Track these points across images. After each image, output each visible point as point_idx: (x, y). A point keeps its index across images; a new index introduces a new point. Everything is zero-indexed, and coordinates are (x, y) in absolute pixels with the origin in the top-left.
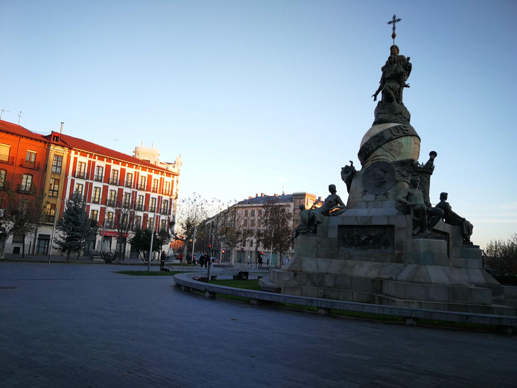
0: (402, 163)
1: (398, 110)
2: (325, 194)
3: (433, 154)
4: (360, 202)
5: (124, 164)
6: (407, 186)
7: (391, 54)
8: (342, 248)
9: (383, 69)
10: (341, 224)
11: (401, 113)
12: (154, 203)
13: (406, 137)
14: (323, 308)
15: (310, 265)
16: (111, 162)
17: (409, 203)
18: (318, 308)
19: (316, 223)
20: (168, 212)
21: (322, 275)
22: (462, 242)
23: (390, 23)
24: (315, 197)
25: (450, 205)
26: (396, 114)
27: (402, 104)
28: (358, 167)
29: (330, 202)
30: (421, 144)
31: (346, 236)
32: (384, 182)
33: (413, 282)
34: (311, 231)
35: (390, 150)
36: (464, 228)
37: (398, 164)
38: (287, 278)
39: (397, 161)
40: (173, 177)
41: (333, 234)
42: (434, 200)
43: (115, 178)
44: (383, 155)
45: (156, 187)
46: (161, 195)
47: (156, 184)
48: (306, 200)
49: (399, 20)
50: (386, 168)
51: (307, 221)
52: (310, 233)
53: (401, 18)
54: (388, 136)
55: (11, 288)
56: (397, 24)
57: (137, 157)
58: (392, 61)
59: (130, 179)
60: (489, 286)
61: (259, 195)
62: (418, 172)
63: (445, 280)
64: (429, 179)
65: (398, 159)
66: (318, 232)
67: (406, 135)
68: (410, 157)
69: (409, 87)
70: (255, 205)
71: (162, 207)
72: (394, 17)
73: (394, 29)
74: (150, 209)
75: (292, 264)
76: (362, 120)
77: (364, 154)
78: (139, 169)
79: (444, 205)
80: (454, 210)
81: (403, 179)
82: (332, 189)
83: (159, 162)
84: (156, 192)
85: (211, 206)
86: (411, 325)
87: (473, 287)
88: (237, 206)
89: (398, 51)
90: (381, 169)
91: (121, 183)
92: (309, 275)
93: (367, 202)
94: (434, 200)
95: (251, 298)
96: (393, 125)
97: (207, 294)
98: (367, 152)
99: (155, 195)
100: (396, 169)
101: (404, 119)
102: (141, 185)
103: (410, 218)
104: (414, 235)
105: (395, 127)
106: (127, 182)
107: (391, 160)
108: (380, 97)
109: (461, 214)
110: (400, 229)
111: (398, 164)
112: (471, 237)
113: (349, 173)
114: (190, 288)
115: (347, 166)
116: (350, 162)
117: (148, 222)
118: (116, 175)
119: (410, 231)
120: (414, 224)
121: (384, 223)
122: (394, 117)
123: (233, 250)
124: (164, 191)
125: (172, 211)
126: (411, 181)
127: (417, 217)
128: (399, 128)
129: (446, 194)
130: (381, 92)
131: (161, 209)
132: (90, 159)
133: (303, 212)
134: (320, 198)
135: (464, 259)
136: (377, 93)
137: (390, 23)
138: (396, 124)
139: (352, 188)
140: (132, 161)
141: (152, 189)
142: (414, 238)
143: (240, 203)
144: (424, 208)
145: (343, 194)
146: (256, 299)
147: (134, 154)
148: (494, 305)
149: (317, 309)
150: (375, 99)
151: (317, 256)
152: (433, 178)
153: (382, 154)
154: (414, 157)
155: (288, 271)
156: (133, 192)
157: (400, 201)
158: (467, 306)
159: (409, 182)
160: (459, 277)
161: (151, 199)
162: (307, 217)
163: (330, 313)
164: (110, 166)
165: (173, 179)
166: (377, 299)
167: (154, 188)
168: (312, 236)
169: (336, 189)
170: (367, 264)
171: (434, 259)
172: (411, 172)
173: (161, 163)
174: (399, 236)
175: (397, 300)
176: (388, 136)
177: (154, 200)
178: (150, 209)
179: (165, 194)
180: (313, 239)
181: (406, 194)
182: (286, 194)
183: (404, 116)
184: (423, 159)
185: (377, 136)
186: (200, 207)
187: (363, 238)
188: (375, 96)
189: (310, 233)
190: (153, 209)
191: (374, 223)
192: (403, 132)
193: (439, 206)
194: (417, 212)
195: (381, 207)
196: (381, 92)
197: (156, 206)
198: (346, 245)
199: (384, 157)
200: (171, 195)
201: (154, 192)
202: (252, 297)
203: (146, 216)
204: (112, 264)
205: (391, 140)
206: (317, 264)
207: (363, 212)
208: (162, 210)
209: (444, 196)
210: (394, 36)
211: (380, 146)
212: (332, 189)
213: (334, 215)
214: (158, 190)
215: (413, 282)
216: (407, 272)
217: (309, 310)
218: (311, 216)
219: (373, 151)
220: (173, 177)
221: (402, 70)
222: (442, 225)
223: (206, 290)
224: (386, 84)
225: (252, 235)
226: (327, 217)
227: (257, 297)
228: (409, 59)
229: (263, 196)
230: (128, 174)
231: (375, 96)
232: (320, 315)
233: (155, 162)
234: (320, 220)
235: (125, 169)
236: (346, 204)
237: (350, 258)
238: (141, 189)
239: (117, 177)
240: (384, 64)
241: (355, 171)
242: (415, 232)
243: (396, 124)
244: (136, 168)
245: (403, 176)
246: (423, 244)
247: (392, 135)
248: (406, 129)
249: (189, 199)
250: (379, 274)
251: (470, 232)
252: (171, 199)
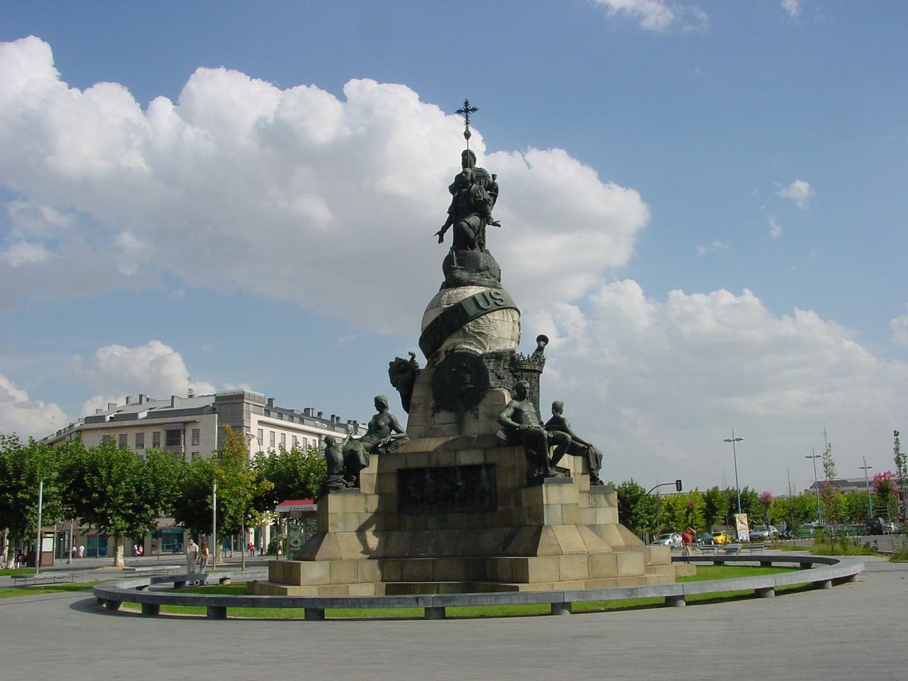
11: (488, 269)
28: (422, 362)
35: (478, 333)
42: (547, 416)
49: (474, 110)
53: (476, 106)
55: (91, 568)
56: (471, 115)
72: (466, 103)
77: (432, 337)
79: (557, 423)
82: (380, 405)
136: (445, 229)
139: (414, 401)
150: (441, 240)
176: (471, 310)
188: (441, 234)
209: (557, 408)
212: (380, 405)
231: (441, 234)
248: (498, 297)
251: (599, 467)
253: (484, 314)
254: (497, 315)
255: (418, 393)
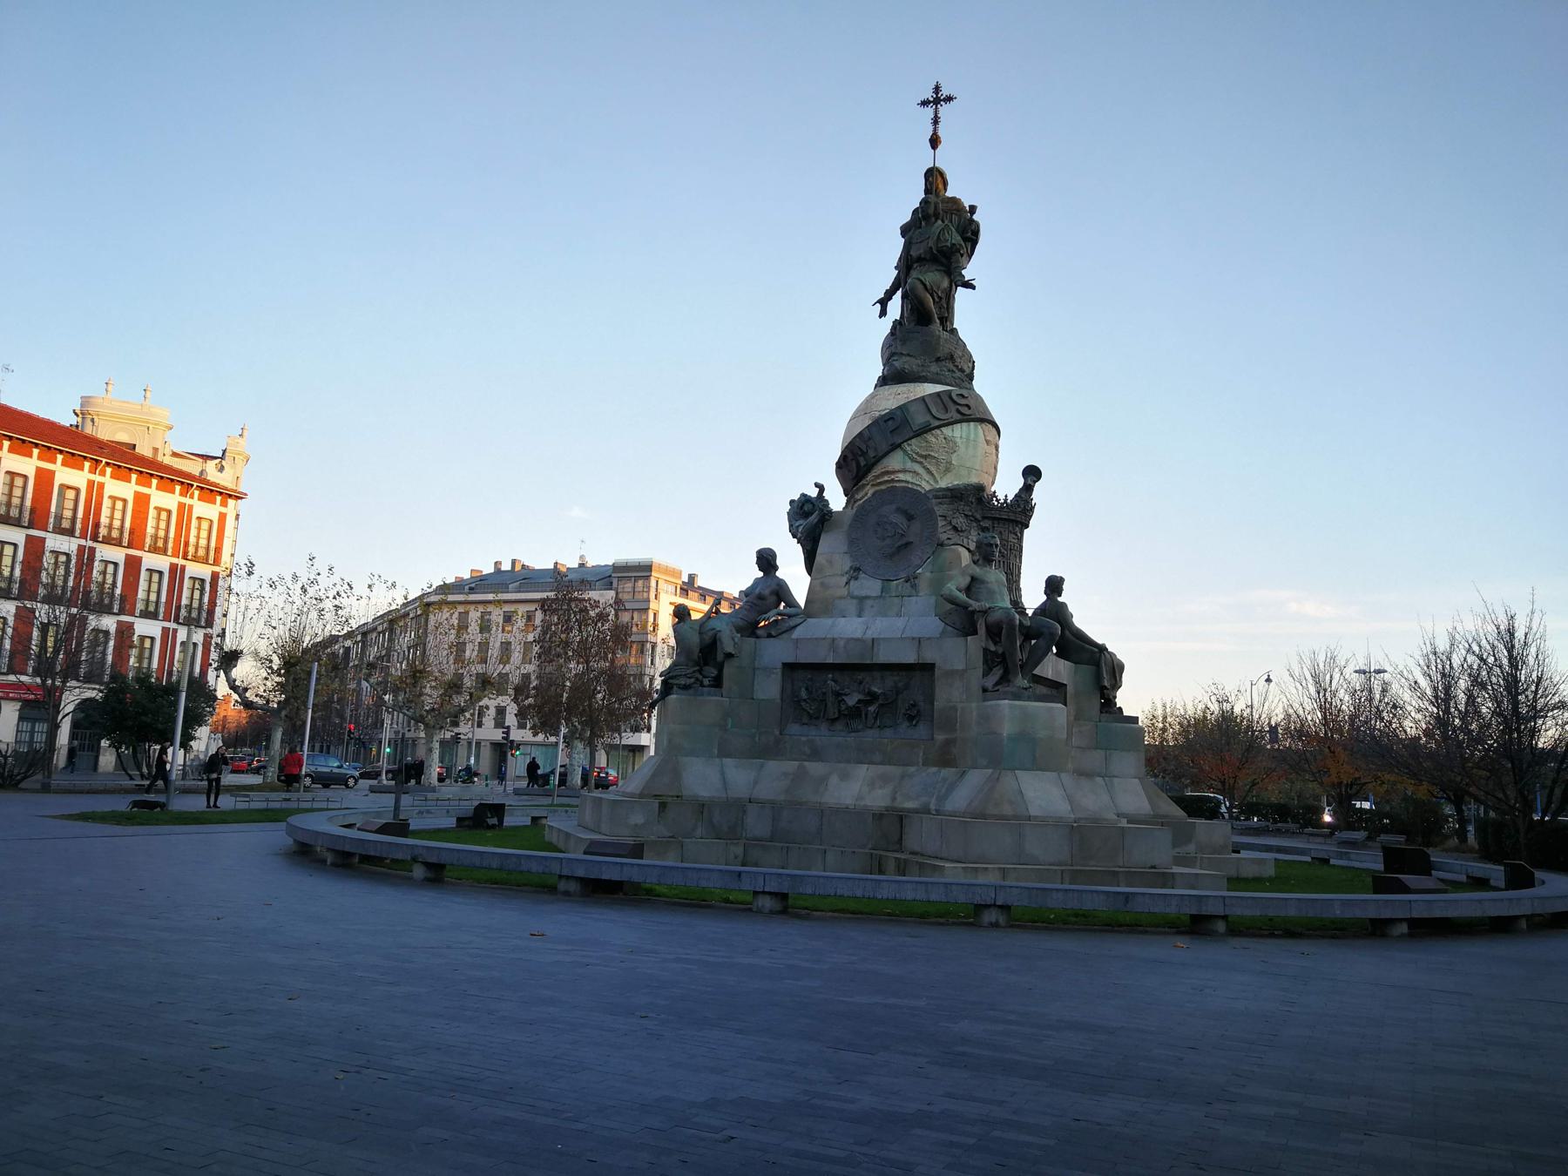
0: (956, 495)
1: (943, 350)
2: (738, 578)
3: (1032, 474)
4: (841, 598)
5: (48, 454)
6: (965, 557)
7: (927, 191)
8: (794, 728)
9: (905, 230)
10: (790, 660)
11: (951, 358)
12: (154, 587)
13: (965, 425)
14: (770, 893)
15: (703, 778)
16: (54, 462)
17: (974, 605)
18: (756, 893)
19: (720, 657)
20: (204, 616)
21: (739, 806)
22: (1098, 707)
23: (925, 103)
24: (678, 574)
25: (1071, 609)
26: (938, 360)
27: (954, 331)
28: (837, 500)
29: (761, 597)
30: (1001, 443)
31: (804, 694)
32: (908, 544)
33: (984, 816)
34: (706, 682)
35: (925, 457)
36: (1101, 669)
37: (945, 497)
38: (637, 819)
39: (941, 489)
40: (224, 504)
41: (769, 689)
42: (1033, 597)
43: (16, 501)
44: (904, 471)
45: (162, 534)
46: (181, 562)
47: (163, 525)
48: (653, 583)
49: (949, 99)
50: (912, 505)
51: (696, 650)
52: (702, 685)
54: (920, 419)
56: (944, 109)
57: (88, 430)
58: (931, 211)
59: (69, 504)
60: (1158, 820)
61: (506, 566)
62: (994, 519)
63: (1062, 808)
64: (1020, 539)
65: (944, 483)
66: (726, 683)
67: (966, 419)
68: (974, 480)
69: (973, 288)
70: (490, 597)
71: (184, 601)
72: (937, 89)
73: (936, 121)
74: (140, 606)
75: (654, 776)
76: (848, 373)
77: (856, 462)
78: (103, 473)
79: (1054, 609)
80: (1079, 622)
81: (956, 539)
82: (766, 560)
83: (168, 452)
84: (164, 552)
85: (364, 601)
86: (995, 925)
87: (1124, 823)
88: (433, 599)
89: (945, 184)
90: (898, 510)
91: (38, 518)
92: (702, 807)
93: (862, 600)
94: (1033, 597)
95: (561, 877)
96: (930, 389)
97: (419, 872)
98: (863, 463)
99: (162, 562)
100: (939, 510)
101: (958, 374)
102: (110, 527)
103: (976, 644)
104: (985, 690)
105: (938, 394)
106: (59, 518)
107: (925, 485)
108: (895, 307)
109: (1096, 634)
110: (951, 673)
111: (945, 497)
112: (1119, 693)
113: (814, 518)
114: (349, 855)
115: (803, 495)
116: (817, 485)
117: (134, 652)
118: (17, 492)
119: (976, 677)
120: (985, 661)
121: (910, 658)
122: (934, 368)
123: (436, 738)
124: (191, 550)
125: (218, 611)
126: (979, 545)
127: (995, 643)
128: (946, 399)
129: (1061, 580)
130: (899, 293)
131: (178, 608)
132: (92, 477)
133: (685, 626)
134: (692, 578)
135: (1102, 752)
136: (889, 295)
137: (925, 103)
138: (939, 388)
140: (73, 442)
141: (148, 541)
142: (985, 700)
143: (444, 588)
144: (1013, 620)
145: (795, 576)
146: (581, 880)
147: (73, 420)
148: (1176, 869)
149: (749, 898)
150: (883, 313)
151: (724, 753)
152: (1031, 538)
153: (901, 468)
154: (985, 480)
155: (641, 796)
156: (81, 549)
157: (951, 600)
158: (1115, 874)
159: (972, 546)
160: (1094, 800)
161: (144, 575)
162: (695, 640)
163: (786, 906)
164: (148, 497)
165: (223, 510)
166: (891, 865)
167: (155, 538)
168: (709, 694)
169: (778, 562)
170: (863, 772)
171: (1037, 755)
172: (977, 520)
173: (175, 455)
174: (948, 695)
175: (947, 865)
176: (920, 419)
177: (156, 577)
178: (140, 606)
179: (196, 559)
180: (711, 705)
181: (965, 581)
182: (591, 563)
183: (958, 366)
184: (1006, 487)
185: (889, 417)
186: (328, 605)
187: (852, 701)
188: (883, 303)
189: (702, 685)
190: (152, 608)
191: (883, 657)
192: (958, 411)
193: (1041, 611)
194: (994, 632)
195: (899, 615)
196: (899, 293)
197: (163, 599)
198: (805, 720)
199: (908, 477)
200: (217, 562)
201: (154, 549)
202: (565, 872)
203: (125, 631)
204: (25, 790)
205: (927, 429)
206: (723, 774)
207: (849, 627)
208: (183, 612)
209: (1054, 586)
210: (934, 142)
211: (899, 446)
212: (766, 560)
213: (770, 636)
214: (170, 545)
215: (984, 816)
216: (965, 792)
217: (727, 901)
218: (707, 638)
219: (878, 460)
220: (224, 504)
221: (957, 239)
222: (1053, 667)
223: (415, 860)
224: (914, 274)
225: (501, 692)
226: (752, 640)
227: (581, 873)
228: (973, 209)
229: (518, 568)
230: (64, 487)
231: (883, 303)
232: (760, 912)
233: (156, 450)
234: (730, 649)
235: (53, 473)
236: (802, 603)
237: (816, 754)
238: (108, 541)
239: (23, 498)
240: (907, 218)
241: (830, 512)
242: (990, 682)
243: (939, 388)
244: (92, 471)
245: (955, 529)
246: (1009, 713)
247: (928, 418)
249: (295, 577)
250: (894, 799)
251: (1117, 684)
252: (215, 576)
253: (938, 427)
254: (958, 432)
255: (826, 544)
